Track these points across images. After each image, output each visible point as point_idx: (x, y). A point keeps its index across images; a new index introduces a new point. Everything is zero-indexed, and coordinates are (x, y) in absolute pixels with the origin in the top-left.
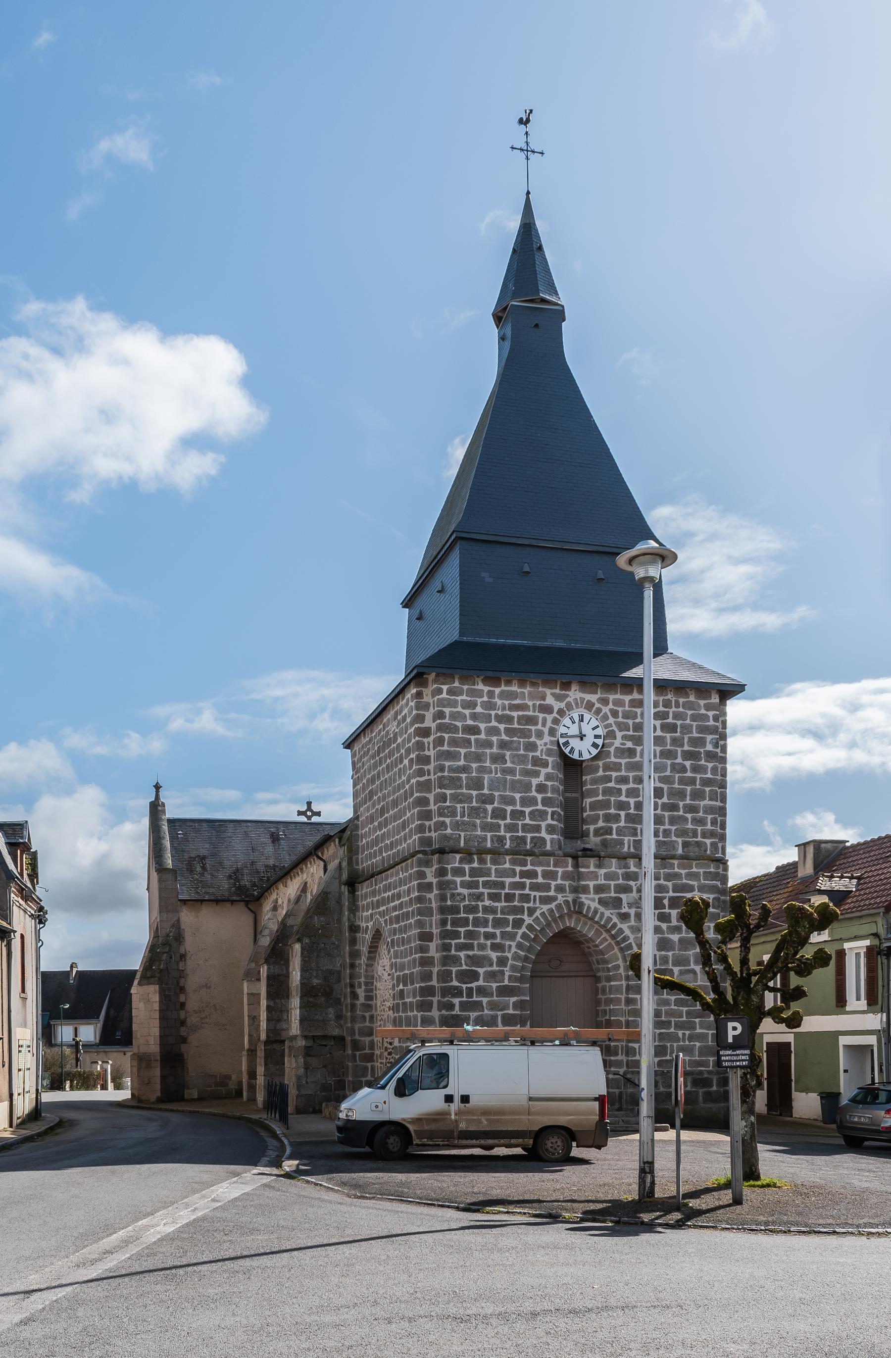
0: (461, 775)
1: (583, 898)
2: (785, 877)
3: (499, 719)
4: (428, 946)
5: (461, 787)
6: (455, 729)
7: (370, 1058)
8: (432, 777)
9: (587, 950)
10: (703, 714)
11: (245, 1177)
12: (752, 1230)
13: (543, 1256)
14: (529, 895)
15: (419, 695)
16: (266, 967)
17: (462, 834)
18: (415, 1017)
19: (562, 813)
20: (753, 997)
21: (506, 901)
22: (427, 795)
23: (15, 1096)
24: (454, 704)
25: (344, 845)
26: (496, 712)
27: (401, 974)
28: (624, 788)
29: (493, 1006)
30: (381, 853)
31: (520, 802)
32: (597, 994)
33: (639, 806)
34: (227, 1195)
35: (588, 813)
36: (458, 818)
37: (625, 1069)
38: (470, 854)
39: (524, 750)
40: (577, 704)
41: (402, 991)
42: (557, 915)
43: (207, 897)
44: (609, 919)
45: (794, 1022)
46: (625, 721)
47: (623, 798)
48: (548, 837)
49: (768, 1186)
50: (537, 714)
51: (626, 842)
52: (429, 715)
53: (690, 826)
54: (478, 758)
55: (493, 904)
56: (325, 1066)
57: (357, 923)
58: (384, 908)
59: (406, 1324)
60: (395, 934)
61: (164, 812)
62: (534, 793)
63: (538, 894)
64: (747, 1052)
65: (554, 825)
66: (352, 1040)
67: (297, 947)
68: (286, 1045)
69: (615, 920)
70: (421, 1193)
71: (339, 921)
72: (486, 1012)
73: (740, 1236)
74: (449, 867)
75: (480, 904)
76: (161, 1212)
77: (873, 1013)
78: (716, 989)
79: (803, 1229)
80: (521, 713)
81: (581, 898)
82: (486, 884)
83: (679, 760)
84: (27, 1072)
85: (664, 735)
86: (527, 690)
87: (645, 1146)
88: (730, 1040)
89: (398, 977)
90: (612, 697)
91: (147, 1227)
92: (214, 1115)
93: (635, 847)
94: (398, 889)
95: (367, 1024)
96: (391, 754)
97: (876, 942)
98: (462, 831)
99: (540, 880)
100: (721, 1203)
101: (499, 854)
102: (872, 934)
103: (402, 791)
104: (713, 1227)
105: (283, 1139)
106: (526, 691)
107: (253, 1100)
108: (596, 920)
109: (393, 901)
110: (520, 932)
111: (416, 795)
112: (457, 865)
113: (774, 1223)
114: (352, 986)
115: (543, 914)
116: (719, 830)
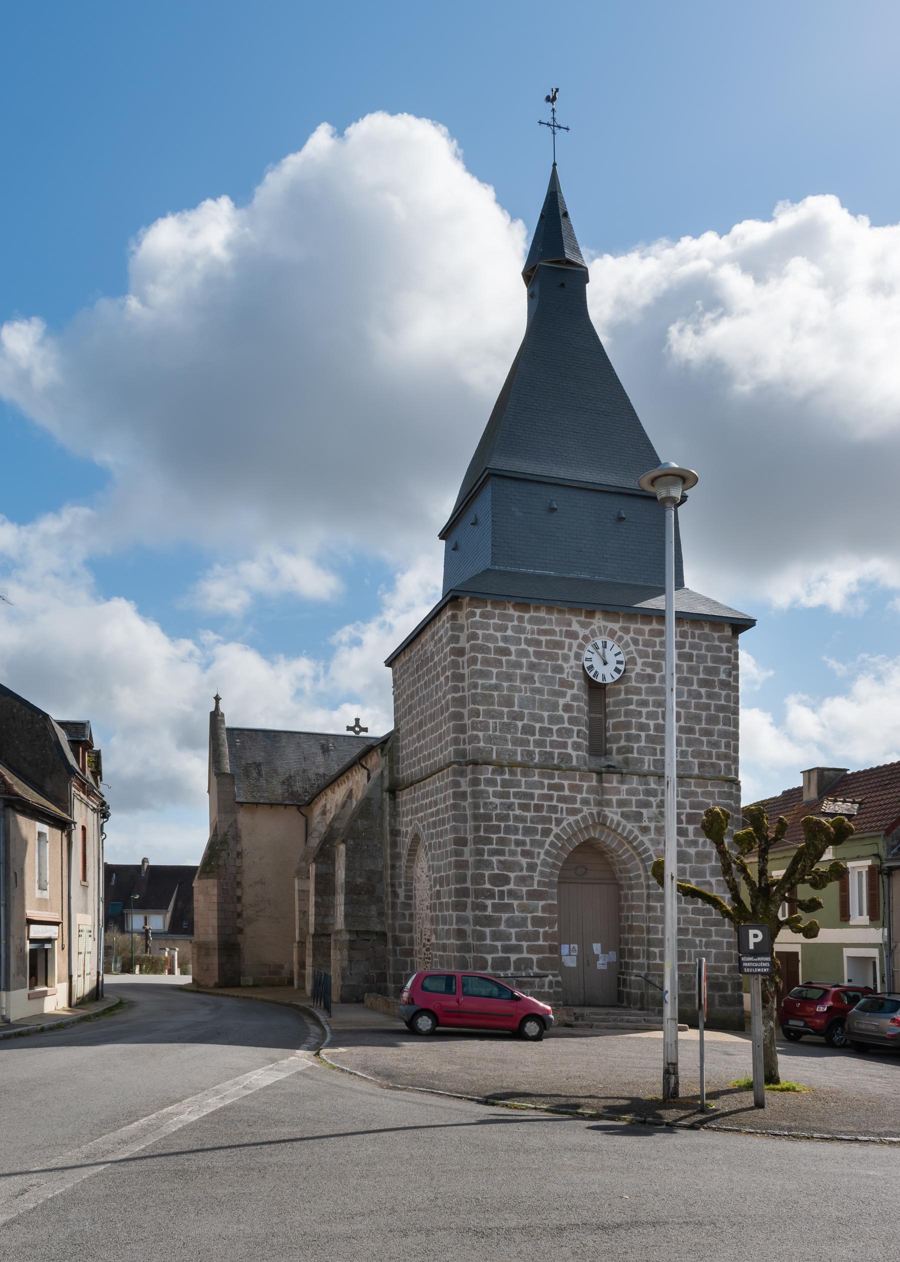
0: (493, 693)
1: (607, 811)
2: (791, 801)
3: (529, 642)
4: (463, 850)
5: (493, 704)
6: (487, 650)
7: (410, 953)
8: (466, 693)
9: (610, 860)
10: (716, 646)
11: (282, 1064)
12: (776, 1135)
13: (569, 1159)
14: (556, 806)
15: (454, 617)
16: (314, 866)
17: (495, 747)
18: (451, 916)
19: (587, 732)
20: (771, 906)
21: (535, 811)
22: (461, 710)
23: (75, 978)
24: (486, 627)
25: (385, 755)
26: (525, 635)
27: (438, 875)
28: (644, 710)
29: (523, 909)
30: (419, 763)
31: (548, 719)
32: (620, 901)
33: (660, 728)
34: (260, 1082)
35: (611, 732)
36: (491, 732)
37: (646, 971)
38: (502, 766)
39: (552, 672)
40: (600, 632)
41: (438, 891)
42: (583, 826)
43: (262, 801)
44: (631, 832)
45: (810, 932)
46: (645, 649)
47: (643, 720)
48: (574, 754)
49: (788, 1090)
50: (563, 639)
51: (646, 761)
52: (463, 636)
53: (705, 748)
54: (509, 677)
55: (523, 813)
56: (368, 959)
57: (398, 828)
58: (423, 814)
59: (422, 1238)
60: (432, 839)
61: (223, 722)
62: (561, 713)
63: (565, 806)
64: (768, 959)
65: (580, 742)
66: (393, 936)
67: (342, 847)
68: (332, 938)
69: (636, 832)
70: (452, 1085)
71: (381, 825)
72: (517, 913)
73: (765, 1141)
74: (482, 777)
75: (511, 813)
76: (189, 1099)
77: (875, 927)
78: (736, 898)
79: (826, 1136)
80: (548, 638)
81: (604, 811)
82: (516, 795)
83: (695, 687)
84: (87, 956)
85: (681, 663)
86: (554, 616)
87: (669, 1048)
88: (751, 947)
89: (435, 878)
90: (633, 626)
91: (171, 1115)
92: (266, 1001)
93: (654, 766)
94: (435, 797)
95: (407, 921)
96: (429, 672)
97: (878, 862)
98: (494, 744)
99: (567, 793)
100: (744, 1106)
101: (529, 768)
102: (874, 855)
103: (439, 706)
104: (737, 1131)
105: (326, 1026)
106: (553, 617)
107: (302, 988)
108: (619, 831)
109: (430, 808)
110: (548, 840)
111: (451, 709)
112: (489, 776)
113: (796, 1128)
114: (393, 886)
115: (569, 825)
116: (732, 754)
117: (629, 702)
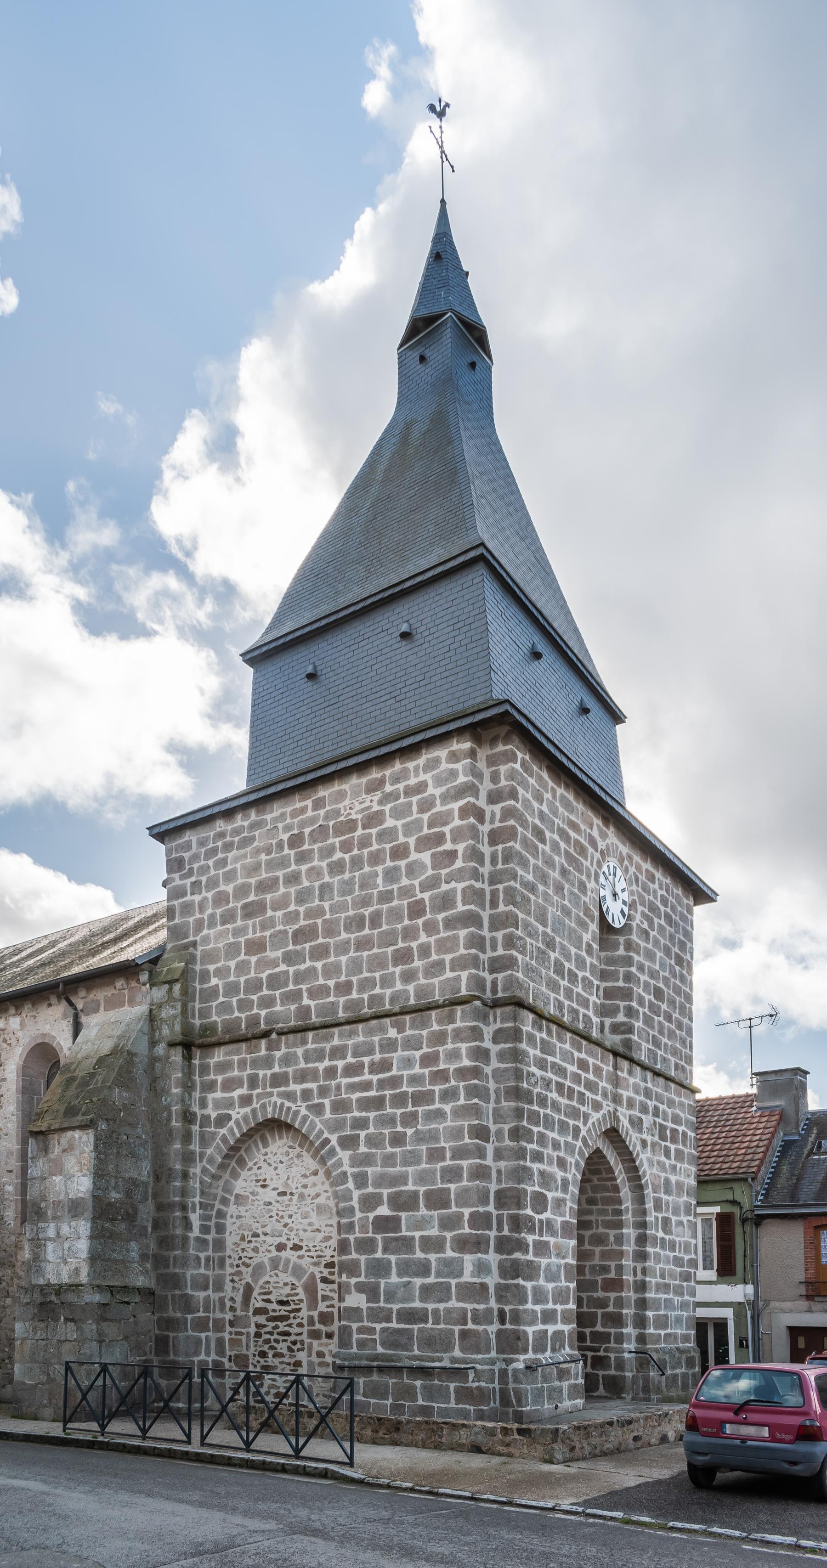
56: (126, 1338)
117: (629, 961)
